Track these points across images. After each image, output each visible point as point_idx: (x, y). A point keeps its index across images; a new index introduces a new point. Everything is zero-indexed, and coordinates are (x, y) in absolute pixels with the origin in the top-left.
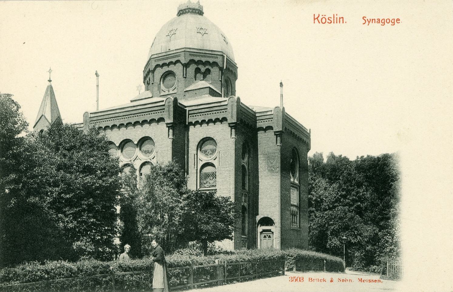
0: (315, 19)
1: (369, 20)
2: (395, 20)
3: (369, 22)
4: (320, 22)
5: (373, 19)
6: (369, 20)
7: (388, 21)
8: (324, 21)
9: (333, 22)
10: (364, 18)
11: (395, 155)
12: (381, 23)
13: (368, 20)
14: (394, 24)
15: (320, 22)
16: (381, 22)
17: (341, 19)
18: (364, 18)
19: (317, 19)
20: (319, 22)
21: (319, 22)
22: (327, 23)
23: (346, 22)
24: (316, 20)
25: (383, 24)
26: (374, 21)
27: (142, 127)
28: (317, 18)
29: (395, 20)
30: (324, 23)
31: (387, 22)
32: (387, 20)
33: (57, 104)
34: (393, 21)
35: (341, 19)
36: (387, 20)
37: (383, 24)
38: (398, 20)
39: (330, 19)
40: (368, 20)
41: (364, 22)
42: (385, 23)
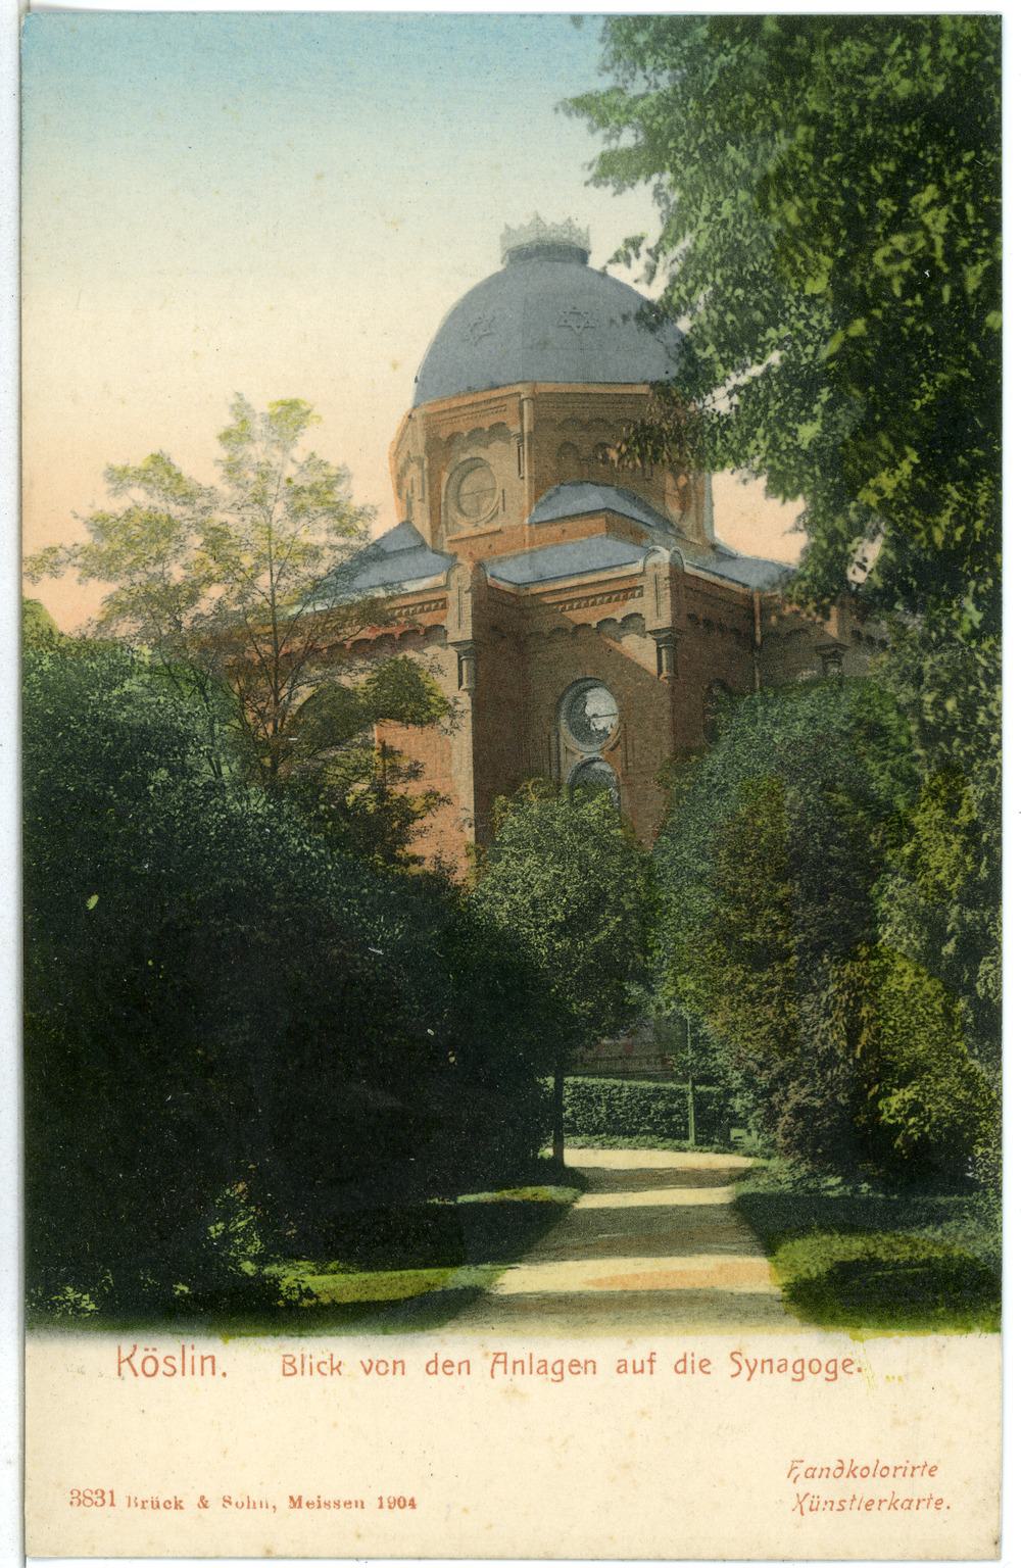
0: (332, 1369)
1: (752, 1364)
2: (566, 1365)
3: (752, 1372)
4: (139, 1370)
5: (205, 1355)
6: (752, 1364)
7: (815, 1366)
8: (150, 1366)
9: (299, 1371)
10: (736, 1357)
11: (77, 606)
12: (551, 1375)
13: (747, 1361)
14: (836, 1378)
15: (139, 1370)
16: (790, 1368)
17: (208, 1363)
18: (736, 1357)
19: (126, 1363)
20: (136, 1375)
21: (136, 1375)
22: (160, 1373)
23: (224, 1374)
24: (125, 1366)
25: (799, 1376)
26: (638, 1368)
27: (80, 582)
28: (337, 1368)
29: (566, 1365)
30: (153, 1375)
31: (387, 1365)
32: (811, 1362)
33: (182, 13)
34: (557, 1368)
35: (399, 1366)
36: (811, 1362)
37: (799, 1376)
38: (704, 1363)
39: (169, 1361)
40: (747, 1361)
41: (736, 1368)
42: (806, 1370)
